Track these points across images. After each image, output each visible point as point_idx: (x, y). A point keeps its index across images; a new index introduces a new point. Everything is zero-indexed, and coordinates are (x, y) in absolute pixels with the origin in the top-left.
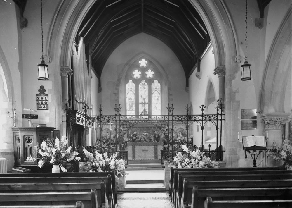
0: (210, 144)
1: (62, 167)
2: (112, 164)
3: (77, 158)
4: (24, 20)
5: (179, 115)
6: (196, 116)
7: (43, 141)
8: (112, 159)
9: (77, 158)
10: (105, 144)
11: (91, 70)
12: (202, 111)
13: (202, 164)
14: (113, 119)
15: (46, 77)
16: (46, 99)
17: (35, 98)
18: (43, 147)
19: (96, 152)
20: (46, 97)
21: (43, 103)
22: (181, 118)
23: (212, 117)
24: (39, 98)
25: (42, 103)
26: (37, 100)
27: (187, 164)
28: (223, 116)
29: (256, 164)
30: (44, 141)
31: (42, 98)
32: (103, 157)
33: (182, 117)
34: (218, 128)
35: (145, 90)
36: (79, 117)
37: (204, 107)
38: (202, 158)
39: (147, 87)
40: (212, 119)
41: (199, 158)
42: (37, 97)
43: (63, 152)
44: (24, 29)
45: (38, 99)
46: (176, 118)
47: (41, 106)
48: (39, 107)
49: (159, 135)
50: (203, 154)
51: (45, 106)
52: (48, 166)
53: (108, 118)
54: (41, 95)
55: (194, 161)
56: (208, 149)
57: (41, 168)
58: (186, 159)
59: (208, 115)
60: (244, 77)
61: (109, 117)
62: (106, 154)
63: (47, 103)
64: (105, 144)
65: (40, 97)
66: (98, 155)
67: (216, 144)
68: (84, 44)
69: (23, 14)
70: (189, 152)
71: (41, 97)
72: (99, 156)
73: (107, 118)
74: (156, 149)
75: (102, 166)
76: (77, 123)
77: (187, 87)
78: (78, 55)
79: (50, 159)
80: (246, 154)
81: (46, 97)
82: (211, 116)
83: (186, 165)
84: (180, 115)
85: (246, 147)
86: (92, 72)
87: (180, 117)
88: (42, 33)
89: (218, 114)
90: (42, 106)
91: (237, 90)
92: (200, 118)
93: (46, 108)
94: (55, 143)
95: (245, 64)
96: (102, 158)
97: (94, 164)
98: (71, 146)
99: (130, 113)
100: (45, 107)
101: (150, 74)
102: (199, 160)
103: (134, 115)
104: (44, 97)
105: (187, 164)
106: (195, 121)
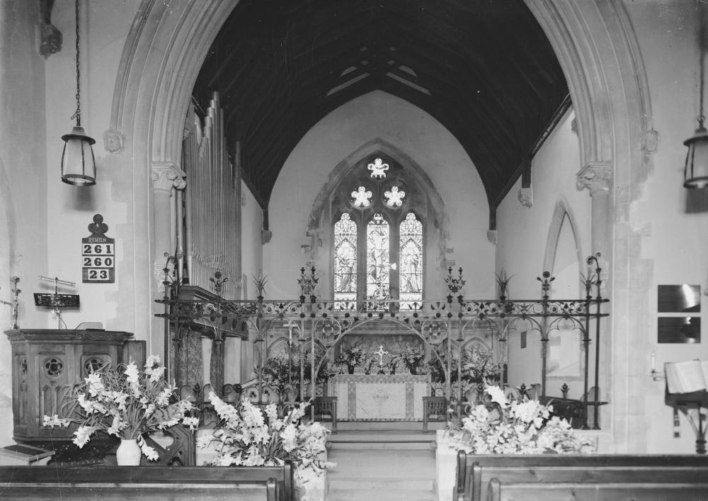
0: (567, 384)
1: (145, 444)
2: (289, 435)
3: (187, 421)
4: (51, 32)
5: (478, 301)
6: (527, 304)
7: (92, 371)
8: (288, 422)
9: (187, 421)
10: (277, 378)
11: (243, 184)
12: (544, 289)
13: (546, 440)
14: (294, 310)
15: (86, 174)
16: (109, 251)
17: (80, 248)
18: (91, 386)
19: (246, 403)
20: (108, 247)
21: (100, 264)
22: (484, 310)
23: (573, 307)
24: (90, 248)
25: (98, 262)
26: (83, 255)
27: (502, 440)
28: (602, 305)
29: (705, 442)
30: (95, 369)
31: (98, 250)
32: (265, 415)
33: (486, 307)
34: (590, 338)
35: (383, 239)
36: (200, 304)
37: (549, 279)
38: (545, 421)
39: (386, 229)
40: (574, 312)
41: (539, 422)
42: (85, 247)
43: (147, 404)
44: (52, 57)
45: (88, 251)
46: (469, 310)
47: (95, 273)
48: (90, 275)
49: (418, 357)
50: (550, 412)
51: (105, 272)
52: (105, 444)
53: (281, 307)
54: (97, 241)
55: (523, 430)
56: (560, 395)
57: (81, 447)
58: (499, 425)
59: (562, 302)
60: (695, 176)
61: (283, 304)
62: (272, 410)
63: (110, 264)
64: (277, 378)
65: (93, 246)
66: (251, 410)
67: (583, 383)
68: (222, 110)
69: (49, 14)
70: (507, 404)
71: (95, 245)
72: (253, 414)
73: (277, 308)
74: (410, 396)
75: (261, 443)
76: (195, 321)
77: (492, 231)
78: (204, 138)
79: (108, 420)
80: (676, 413)
81: (108, 247)
82: (569, 303)
83: (499, 443)
84: (482, 301)
85: (678, 395)
86: (245, 190)
87: (482, 307)
88: (77, 43)
89: (589, 297)
90: (98, 271)
91: (646, 230)
92: (539, 308)
93: (107, 279)
94: (126, 376)
95: (700, 135)
96: (261, 420)
97: (238, 437)
98: (172, 386)
99: (345, 299)
100: (106, 277)
101: (395, 197)
102: (537, 429)
103: (353, 301)
104: (104, 247)
105: (502, 440)
106: (524, 316)
